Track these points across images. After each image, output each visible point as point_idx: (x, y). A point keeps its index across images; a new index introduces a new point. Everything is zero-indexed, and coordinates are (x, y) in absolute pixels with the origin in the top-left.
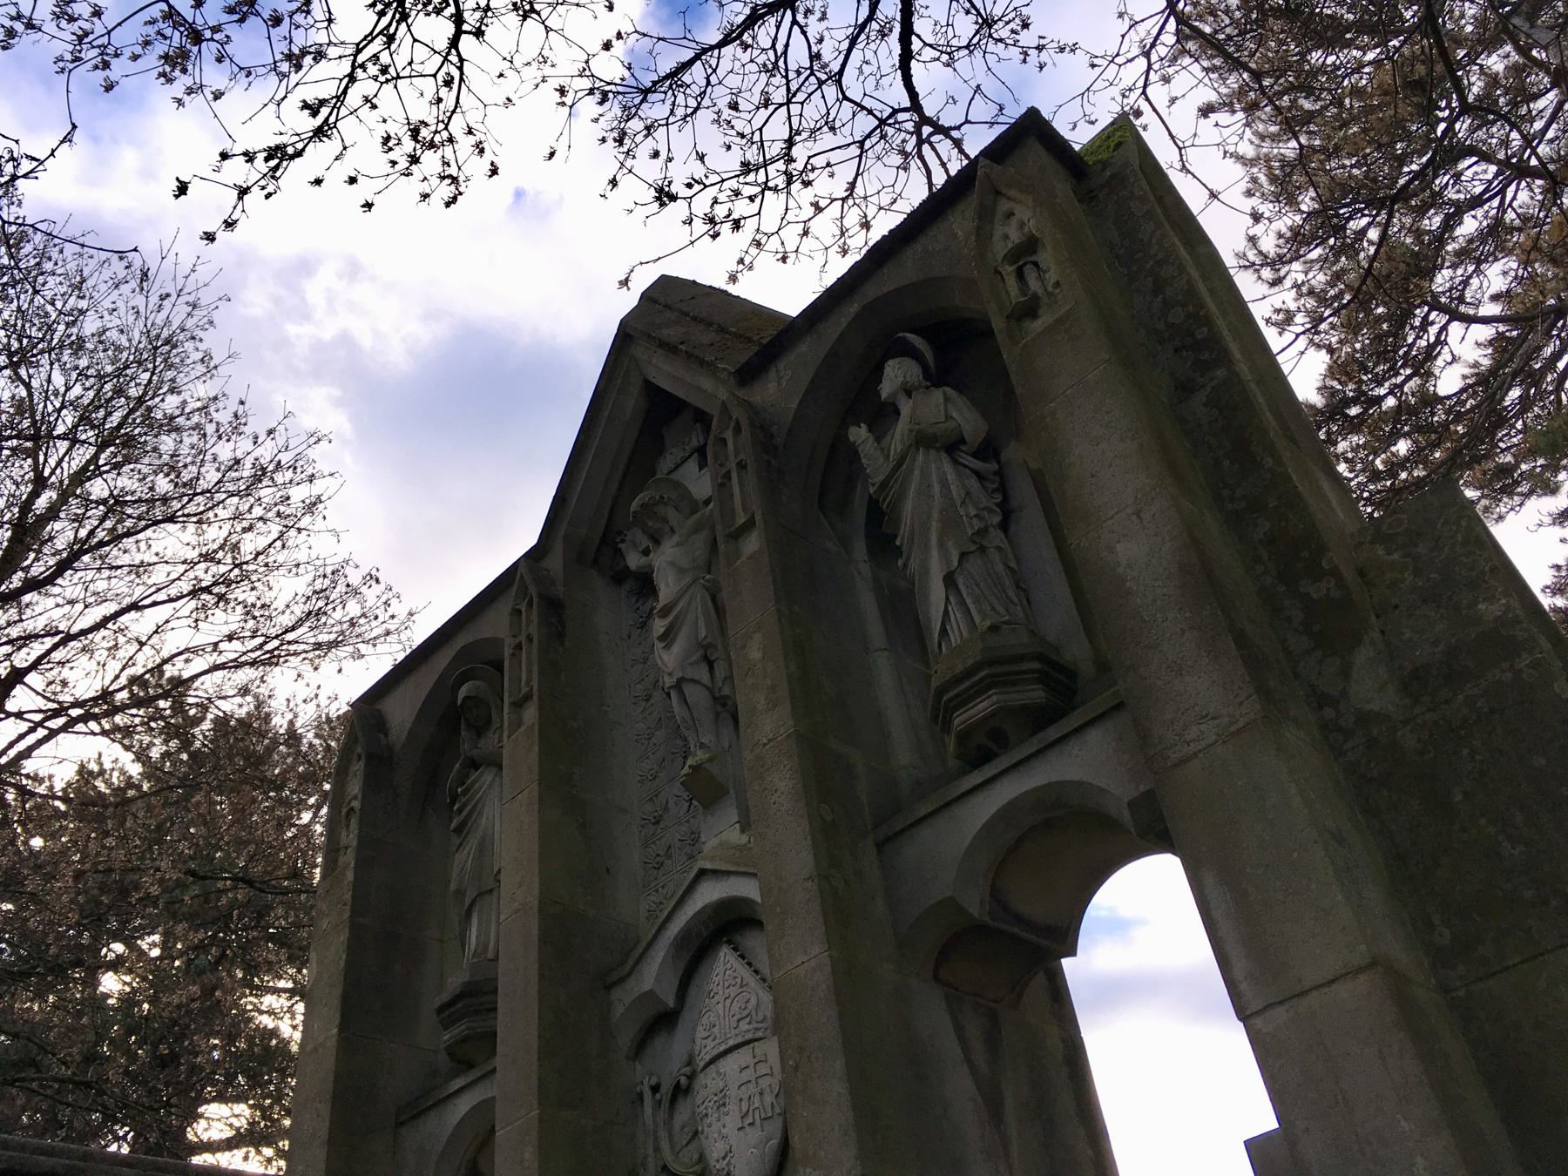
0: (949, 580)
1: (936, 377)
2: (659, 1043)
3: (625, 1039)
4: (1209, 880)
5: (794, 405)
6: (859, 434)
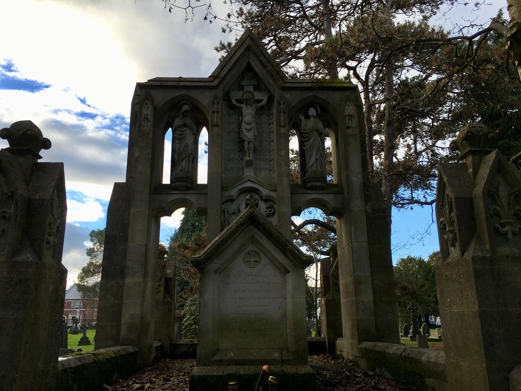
0: (316, 160)
1: (318, 116)
2: (229, 204)
3: (223, 201)
4: (148, 111)
5: (293, 104)
6: (302, 117)
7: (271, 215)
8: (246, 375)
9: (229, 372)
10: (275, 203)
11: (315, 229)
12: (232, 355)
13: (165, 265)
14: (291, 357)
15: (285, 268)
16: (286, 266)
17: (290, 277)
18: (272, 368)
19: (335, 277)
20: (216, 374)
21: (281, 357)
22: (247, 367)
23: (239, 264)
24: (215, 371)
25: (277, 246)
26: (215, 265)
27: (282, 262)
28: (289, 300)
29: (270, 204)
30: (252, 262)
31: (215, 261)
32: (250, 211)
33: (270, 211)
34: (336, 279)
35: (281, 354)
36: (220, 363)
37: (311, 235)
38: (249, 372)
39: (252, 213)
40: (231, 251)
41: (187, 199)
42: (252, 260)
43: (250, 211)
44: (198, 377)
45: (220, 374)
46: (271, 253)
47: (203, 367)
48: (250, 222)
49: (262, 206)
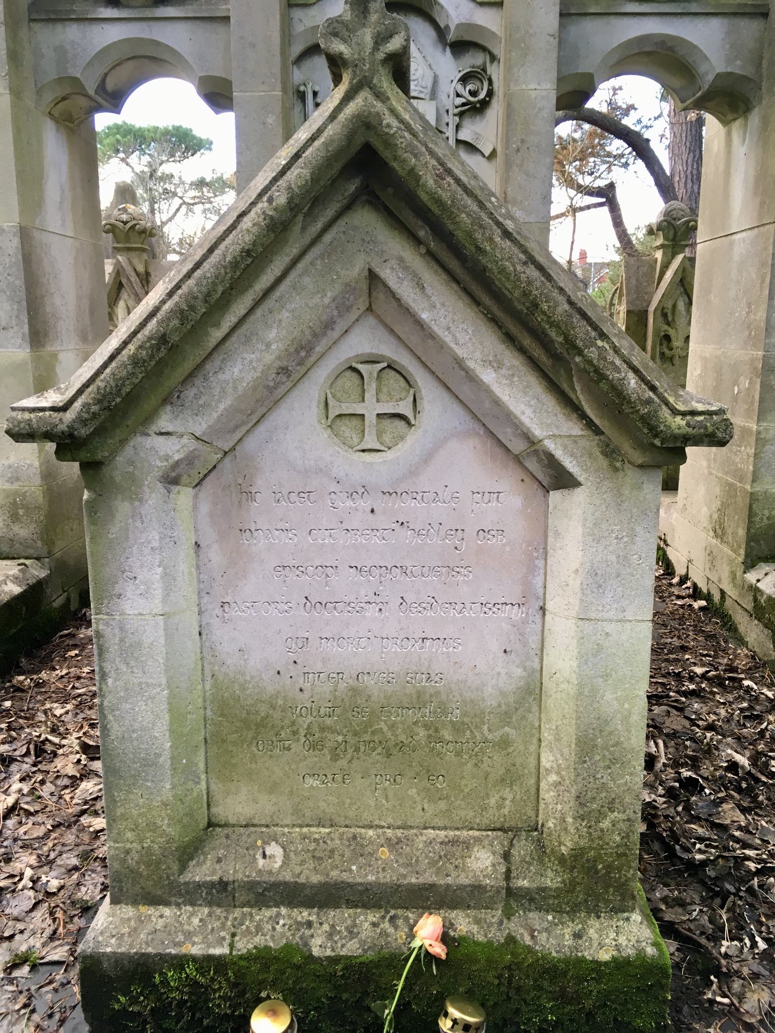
3: (297, 49)
7: (475, 109)
8: (334, 960)
9: (259, 940)
10: (493, 58)
11: (575, 131)
12: (273, 860)
13: (148, 274)
14: (552, 880)
15: (551, 462)
16: (559, 454)
17: (573, 512)
18: (464, 924)
19: (665, 315)
20: (196, 950)
21: (508, 876)
22: (341, 917)
23: (299, 433)
24: (192, 933)
25: (510, 339)
26: (164, 442)
27: (538, 432)
28: (562, 631)
29: (473, 60)
30: (371, 419)
31: (164, 422)
32: (351, 109)
33: (473, 93)
34: (668, 324)
35: (506, 856)
36: (221, 893)
37: (564, 148)
38: (351, 948)
39: (366, 123)
40: (241, 369)
41: (157, 43)
42: (371, 408)
43: (351, 109)
44: (117, 959)
45: (217, 951)
46: (471, 377)
47: (143, 909)
48: (352, 187)
49: (434, 70)
